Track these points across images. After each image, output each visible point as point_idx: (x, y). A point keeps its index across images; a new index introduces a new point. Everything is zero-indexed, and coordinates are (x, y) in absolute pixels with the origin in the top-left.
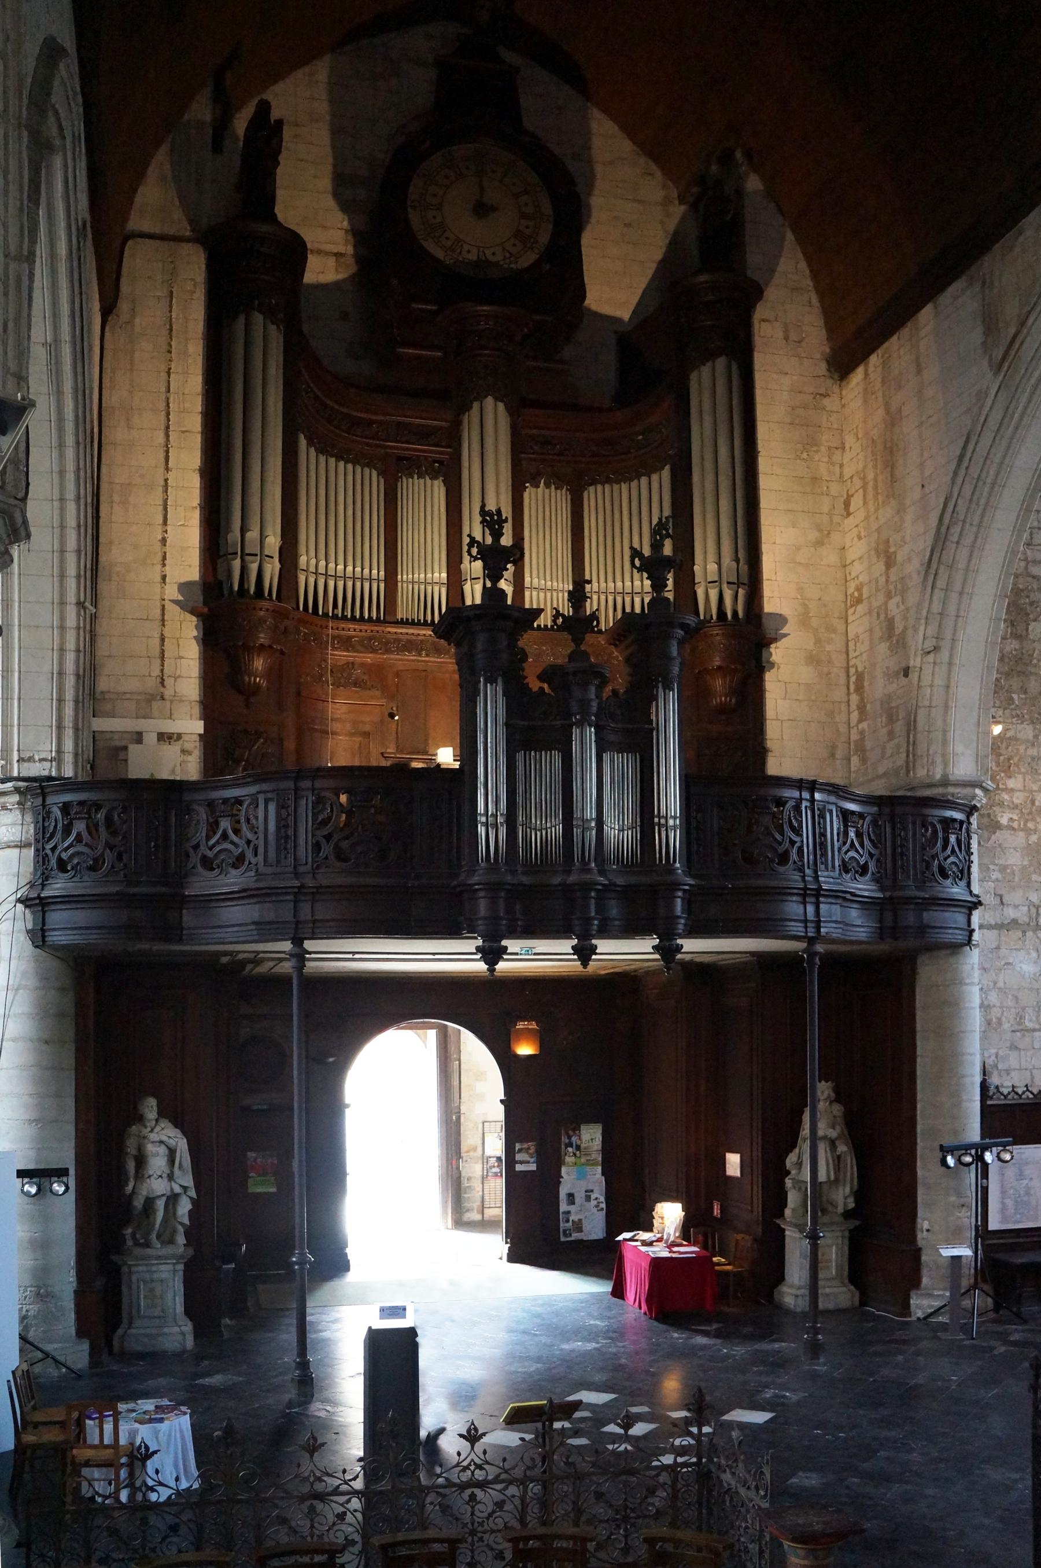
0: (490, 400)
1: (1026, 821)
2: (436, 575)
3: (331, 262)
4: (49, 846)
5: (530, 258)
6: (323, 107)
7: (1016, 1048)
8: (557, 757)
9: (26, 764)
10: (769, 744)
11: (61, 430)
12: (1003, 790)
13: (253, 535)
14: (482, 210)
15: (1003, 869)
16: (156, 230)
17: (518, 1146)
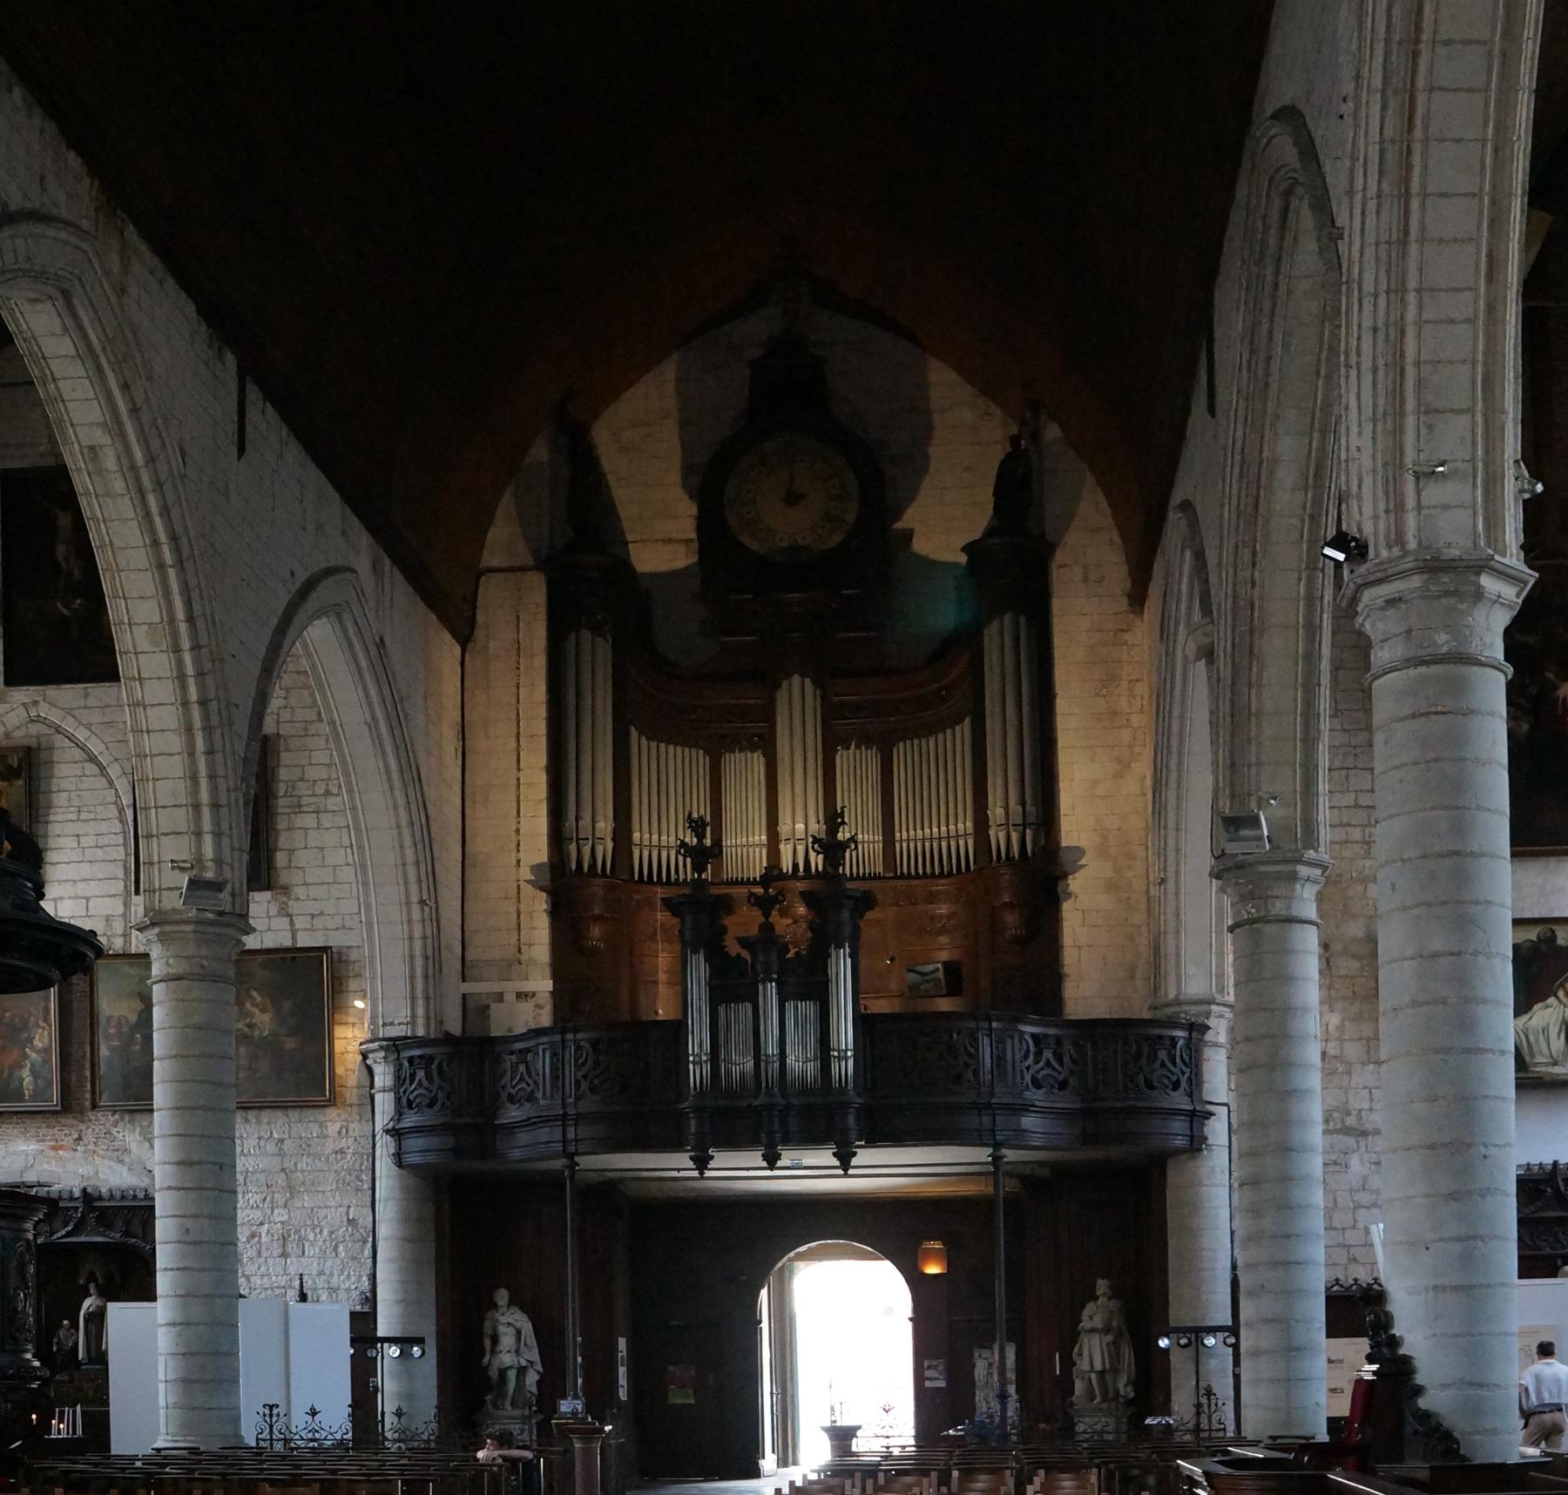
0: (796, 679)
3: (682, 549)
5: (837, 538)
8: (749, 1006)
11: (389, 779)
13: (586, 821)
16: (505, 564)
17: (926, 1364)
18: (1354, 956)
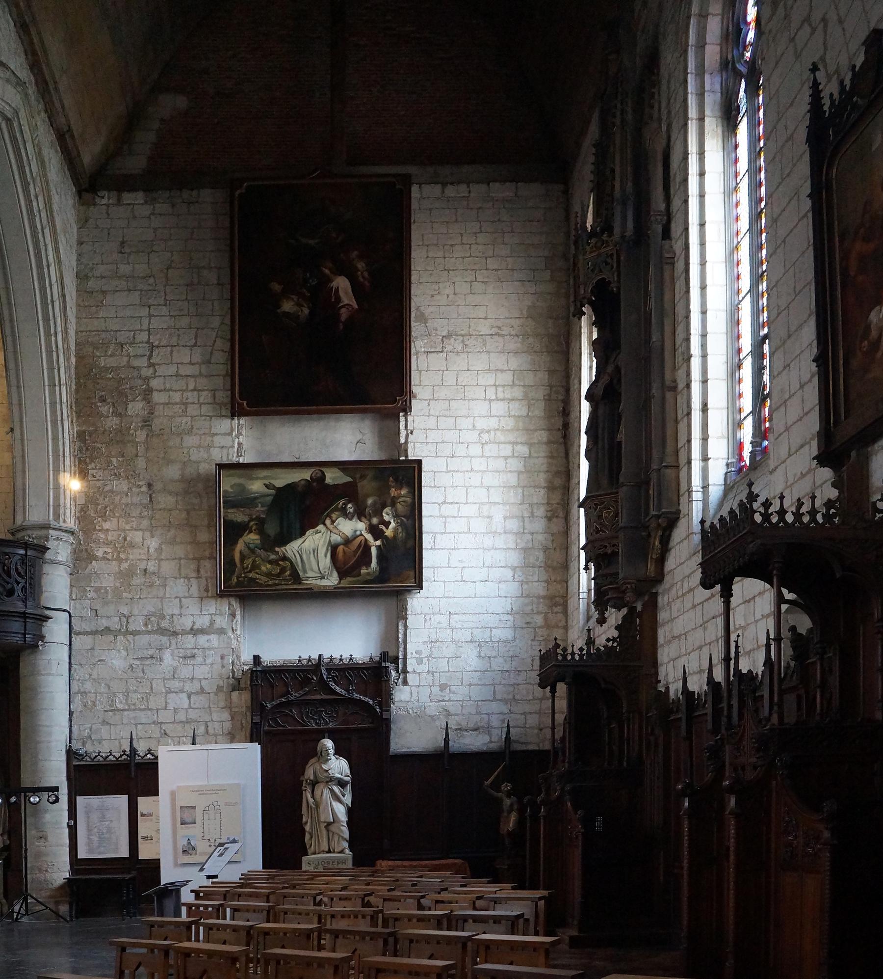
1: (119, 553)
7: (108, 723)
12: (99, 530)
15: (98, 590)
18: (170, 493)
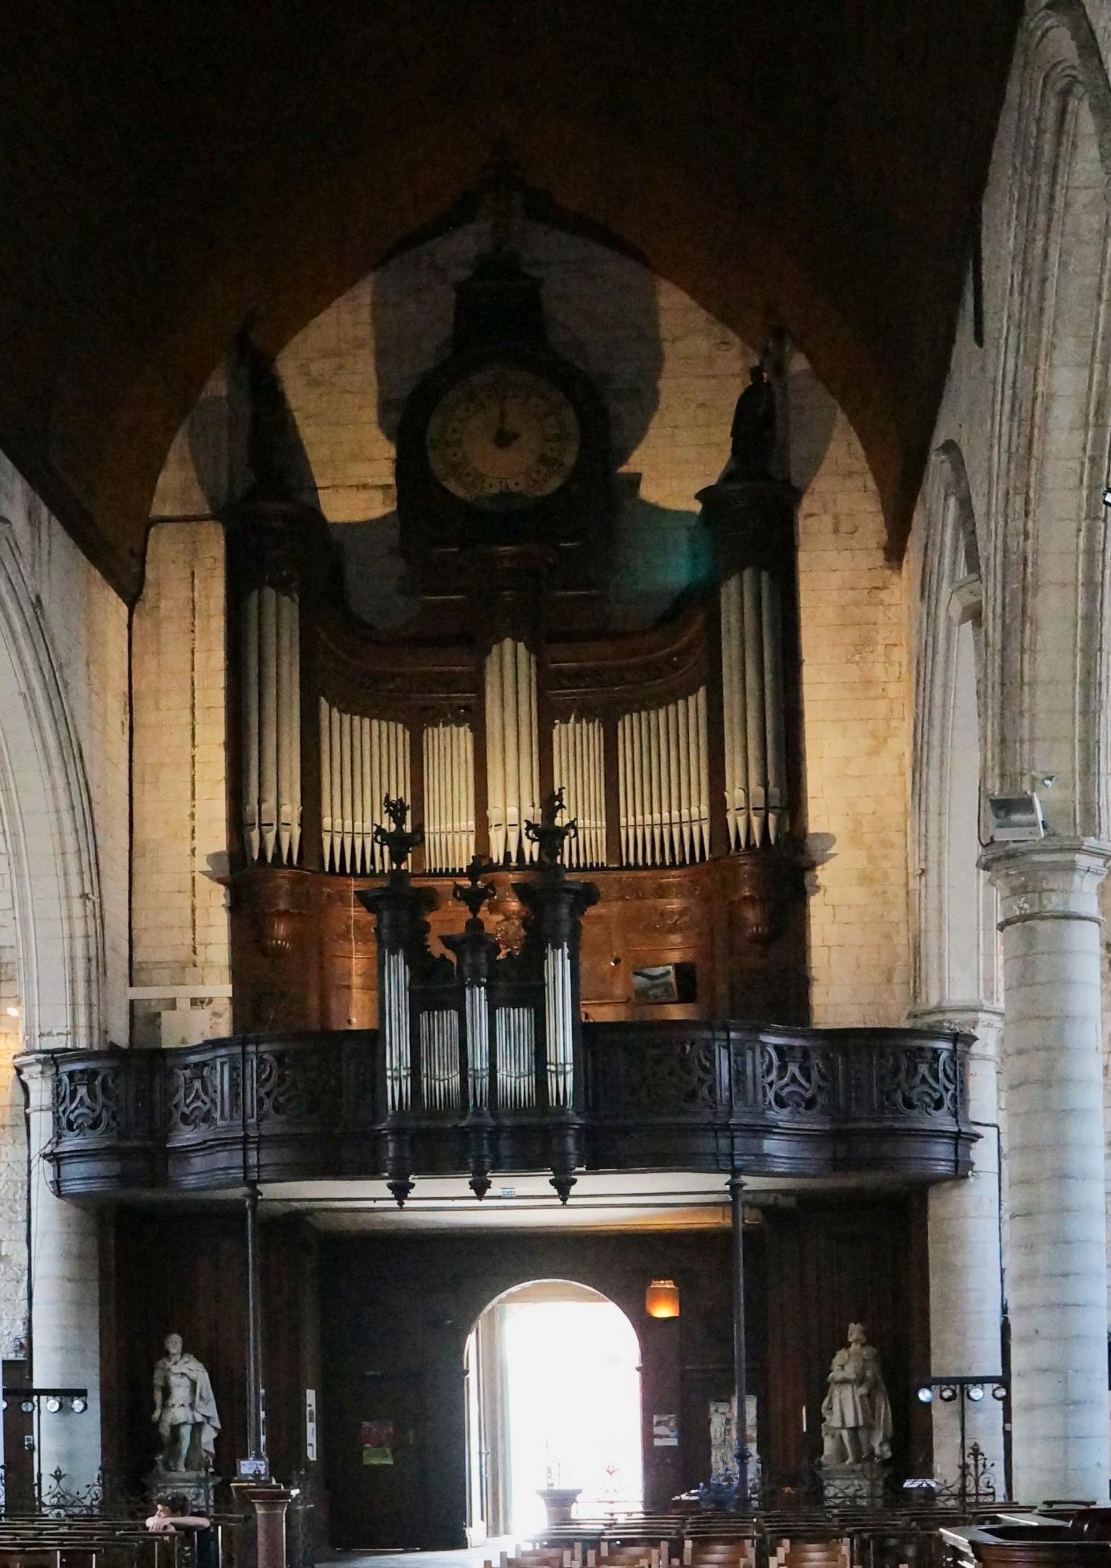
0: (508, 643)
2: (463, 823)
3: (378, 496)
4: (61, 1109)
6: (366, 331)
8: (454, 1014)
9: (45, 1038)
10: (814, 973)
13: (270, 804)
14: (504, 439)
16: (178, 513)
17: (656, 1419)
